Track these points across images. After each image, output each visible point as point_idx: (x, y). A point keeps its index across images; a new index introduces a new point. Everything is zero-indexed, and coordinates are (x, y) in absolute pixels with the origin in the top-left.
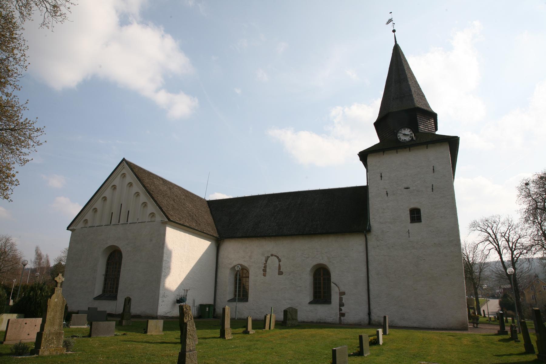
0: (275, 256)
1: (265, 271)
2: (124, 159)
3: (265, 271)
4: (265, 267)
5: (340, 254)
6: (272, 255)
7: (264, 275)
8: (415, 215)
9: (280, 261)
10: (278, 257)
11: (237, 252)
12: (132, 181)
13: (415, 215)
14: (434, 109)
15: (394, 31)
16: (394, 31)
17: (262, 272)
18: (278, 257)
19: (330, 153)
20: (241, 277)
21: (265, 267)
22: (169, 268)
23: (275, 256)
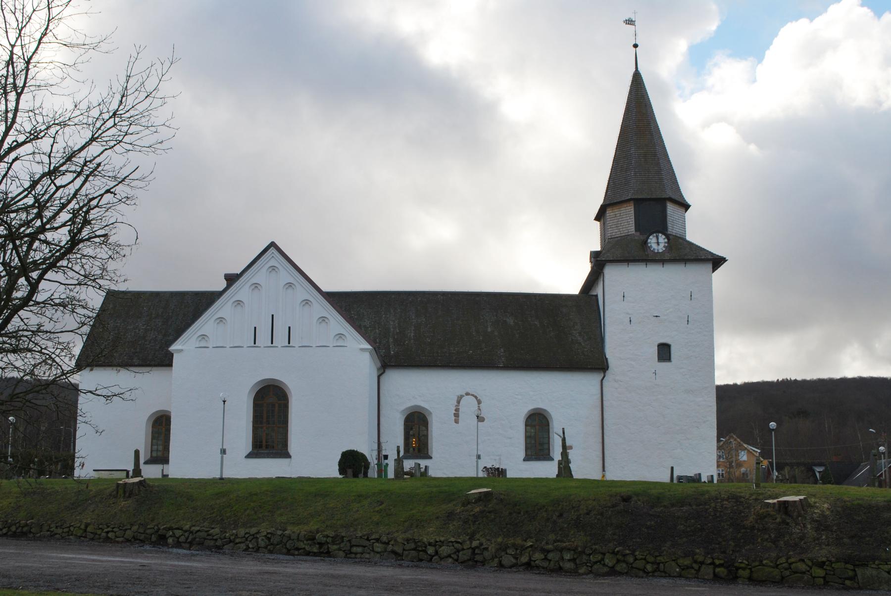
0: (473, 395)
1: (456, 415)
2: (273, 245)
3: (456, 415)
4: (457, 410)
5: (562, 395)
6: (467, 394)
7: (457, 422)
8: (664, 352)
9: (479, 402)
10: (476, 397)
11: (415, 387)
12: (291, 280)
13: (664, 352)
14: (689, 199)
15: (636, 46)
16: (636, 46)
17: (454, 418)
18: (476, 397)
19: (546, 254)
20: (417, 424)
21: (457, 410)
22: (412, 407)
23: (473, 395)
